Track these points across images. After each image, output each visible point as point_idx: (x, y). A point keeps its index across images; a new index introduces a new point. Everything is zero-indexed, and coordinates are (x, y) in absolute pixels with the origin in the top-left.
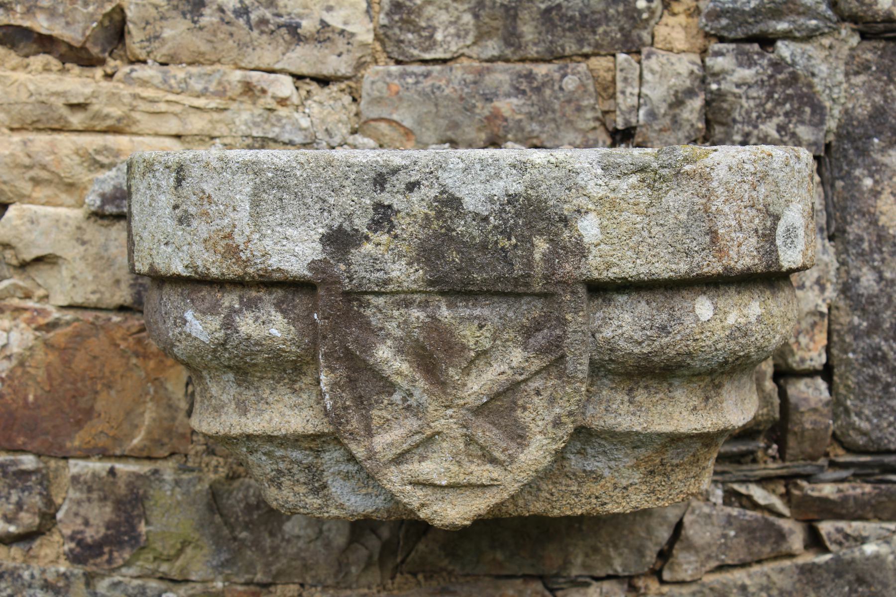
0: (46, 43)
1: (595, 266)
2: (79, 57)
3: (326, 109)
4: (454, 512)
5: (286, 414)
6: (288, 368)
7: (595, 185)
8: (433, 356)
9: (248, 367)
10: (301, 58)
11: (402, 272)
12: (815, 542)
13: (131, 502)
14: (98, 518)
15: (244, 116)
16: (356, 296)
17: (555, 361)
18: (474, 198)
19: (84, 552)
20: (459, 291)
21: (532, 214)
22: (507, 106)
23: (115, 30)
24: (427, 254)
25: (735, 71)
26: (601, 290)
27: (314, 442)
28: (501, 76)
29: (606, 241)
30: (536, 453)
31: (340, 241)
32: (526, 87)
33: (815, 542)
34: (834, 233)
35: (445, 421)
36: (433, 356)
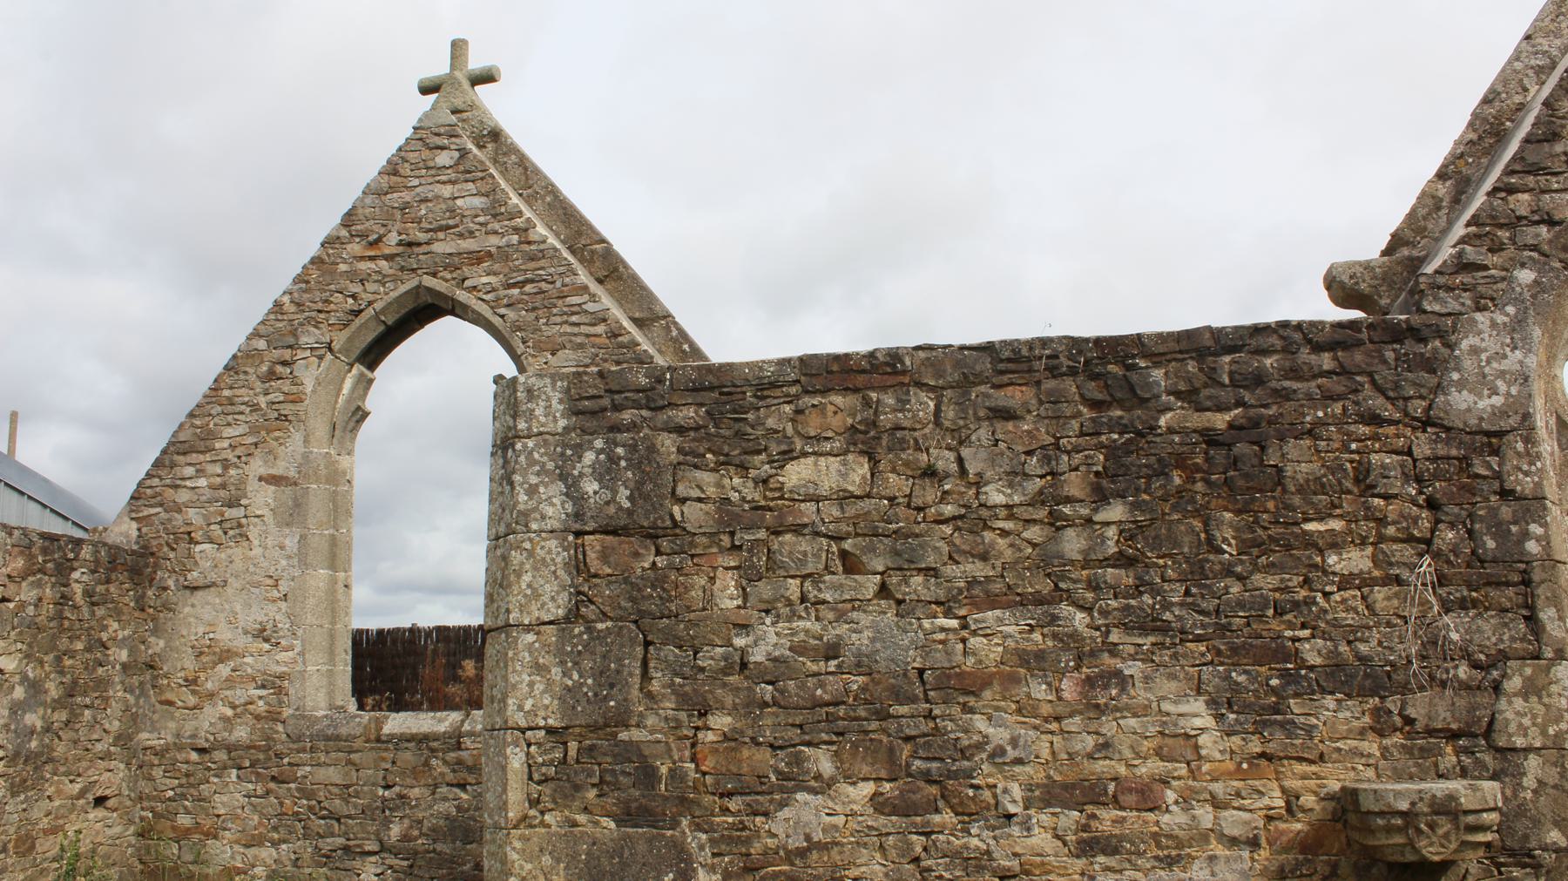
1: (1464, 807)
6: (1399, 830)
7: (1463, 792)
8: (1432, 826)
9: (1389, 830)
10: (1363, 761)
12: (1500, 873)
13: (1334, 867)
14: (1327, 870)
16: (1417, 815)
17: (1458, 828)
18: (1439, 794)
20: (1437, 813)
23: (1322, 756)
24: (1430, 806)
25: (1466, 760)
26: (1466, 812)
28: (1411, 763)
29: (1466, 802)
30: (1453, 846)
31: (1413, 804)
32: (1417, 765)
33: (1500, 873)
34: (817, 793)
35: (1434, 839)
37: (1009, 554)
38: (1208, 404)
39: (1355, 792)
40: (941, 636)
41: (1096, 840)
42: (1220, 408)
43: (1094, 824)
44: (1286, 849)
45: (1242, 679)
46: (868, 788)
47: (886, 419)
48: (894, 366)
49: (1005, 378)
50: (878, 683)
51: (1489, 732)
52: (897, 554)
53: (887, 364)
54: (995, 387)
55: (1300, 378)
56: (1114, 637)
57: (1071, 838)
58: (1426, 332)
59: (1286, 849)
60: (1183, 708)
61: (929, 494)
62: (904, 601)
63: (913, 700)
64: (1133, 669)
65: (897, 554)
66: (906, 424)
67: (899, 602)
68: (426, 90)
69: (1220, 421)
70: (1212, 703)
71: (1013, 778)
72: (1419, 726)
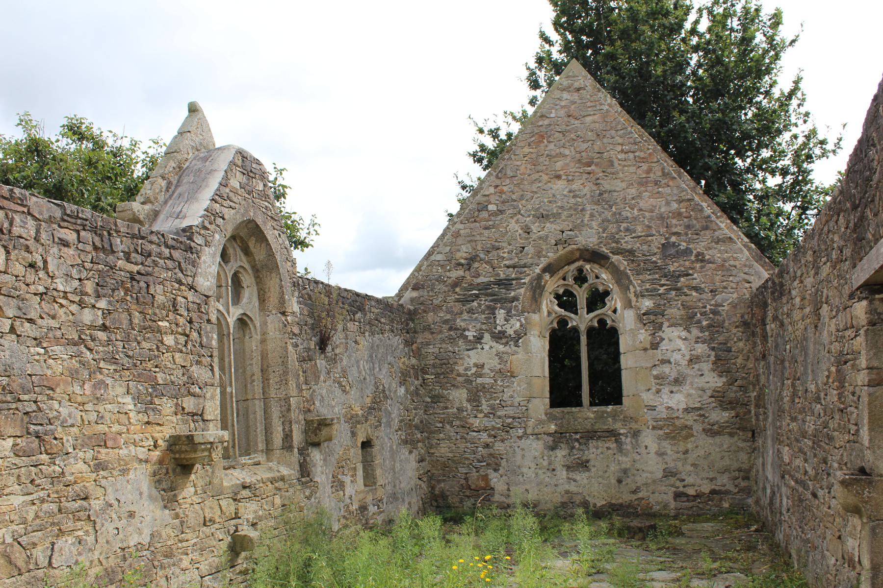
37: (64, 318)
38: (133, 260)
39: (192, 436)
40: (37, 357)
41: (100, 464)
42: (136, 264)
43: (99, 456)
44: (155, 464)
45: (141, 388)
46: (10, 442)
47: (16, 231)
48: (22, 201)
49: (66, 224)
50: (14, 382)
51: (201, 415)
52: (20, 309)
53: (20, 199)
54: (60, 226)
55: (160, 258)
56: (102, 364)
57: (91, 463)
58: (194, 250)
59: (155, 464)
60: (124, 401)
61: (31, 277)
62: (21, 336)
63: (29, 392)
64: (109, 381)
65: (20, 309)
66: (24, 236)
67: (18, 336)
68: (306, 269)
69: (136, 268)
70: (133, 398)
71: (69, 434)
72: (186, 411)
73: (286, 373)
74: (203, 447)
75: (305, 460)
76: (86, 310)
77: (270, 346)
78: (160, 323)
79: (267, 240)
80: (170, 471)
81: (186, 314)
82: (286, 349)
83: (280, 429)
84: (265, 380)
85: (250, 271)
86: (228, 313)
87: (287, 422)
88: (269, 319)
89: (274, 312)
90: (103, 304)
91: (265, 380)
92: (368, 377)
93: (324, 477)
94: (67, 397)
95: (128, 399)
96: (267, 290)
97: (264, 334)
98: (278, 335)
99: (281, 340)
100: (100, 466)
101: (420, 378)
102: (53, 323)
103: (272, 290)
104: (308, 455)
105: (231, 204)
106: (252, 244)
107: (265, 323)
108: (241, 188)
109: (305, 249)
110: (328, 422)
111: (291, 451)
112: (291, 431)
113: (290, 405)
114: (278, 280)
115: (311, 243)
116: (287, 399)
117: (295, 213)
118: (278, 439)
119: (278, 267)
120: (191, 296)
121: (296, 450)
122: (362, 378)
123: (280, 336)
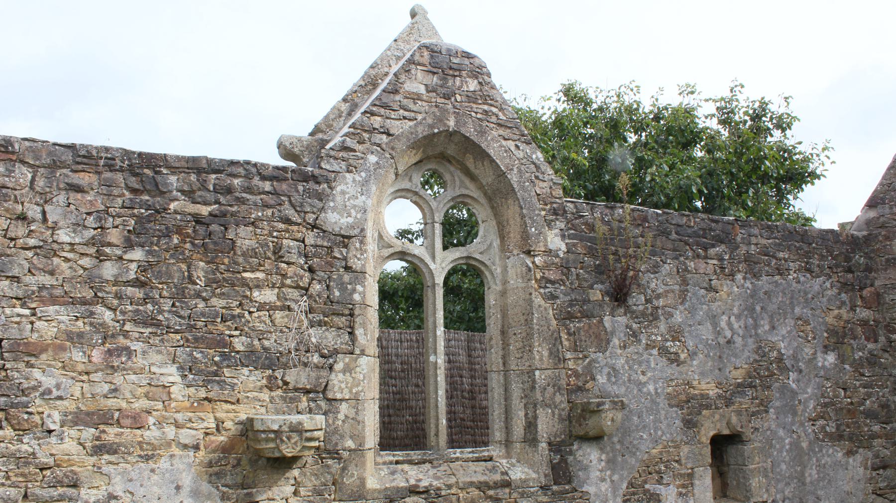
0: (230, 402)
2: (233, 403)
3: (263, 410)
4: (290, 455)
5: (272, 445)
6: (273, 440)
8: (289, 438)
10: (260, 403)
11: (287, 429)
13: (239, 460)
15: (254, 410)
17: (301, 439)
18: (294, 422)
19: (234, 467)
20: (292, 431)
21: (300, 423)
22: (285, 409)
23: (238, 400)
25: (312, 405)
26: (306, 431)
27: (274, 448)
29: (307, 426)
30: (298, 448)
31: (280, 426)
32: (288, 407)
36: (289, 438)
37: (68, 273)
42: (206, 203)
43: (103, 436)
44: (214, 451)
45: (199, 356)
48: (7, 147)
49: (80, 167)
54: (73, 171)
55: (252, 193)
58: (320, 179)
59: (214, 451)
64: (137, 346)
69: (205, 210)
70: (181, 368)
72: (291, 386)
73: (529, 336)
74: (263, 436)
75: (563, 460)
76: (108, 264)
77: (511, 299)
78: (246, 275)
79: (488, 156)
80: (244, 462)
81: (302, 261)
82: (530, 302)
83: (522, 414)
84: (505, 345)
85: (483, 200)
86: (433, 258)
87: (531, 406)
88: (510, 263)
89: (515, 252)
90: (137, 254)
91: (505, 345)
92: (739, 340)
93: (605, 487)
94: (60, 365)
95: (173, 369)
96: (505, 223)
97: (505, 282)
98: (520, 283)
99: (524, 289)
100: (100, 449)
101: (882, 339)
102: (47, 280)
103: (512, 222)
104: (571, 453)
105: (406, 114)
106: (470, 163)
107: (505, 269)
108: (428, 92)
109: (816, 181)
110: (593, 407)
111: (536, 446)
112: (536, 417)
113: (534, 381)
114: (517, 208)
115: (824, 173)
116: (531, 373)
117: (800, 143)
118: (518, 429)
119: (513, 189)
120: (311, 238)
121: (544, 445)
122: (722, 341)
123: (523, 285)
